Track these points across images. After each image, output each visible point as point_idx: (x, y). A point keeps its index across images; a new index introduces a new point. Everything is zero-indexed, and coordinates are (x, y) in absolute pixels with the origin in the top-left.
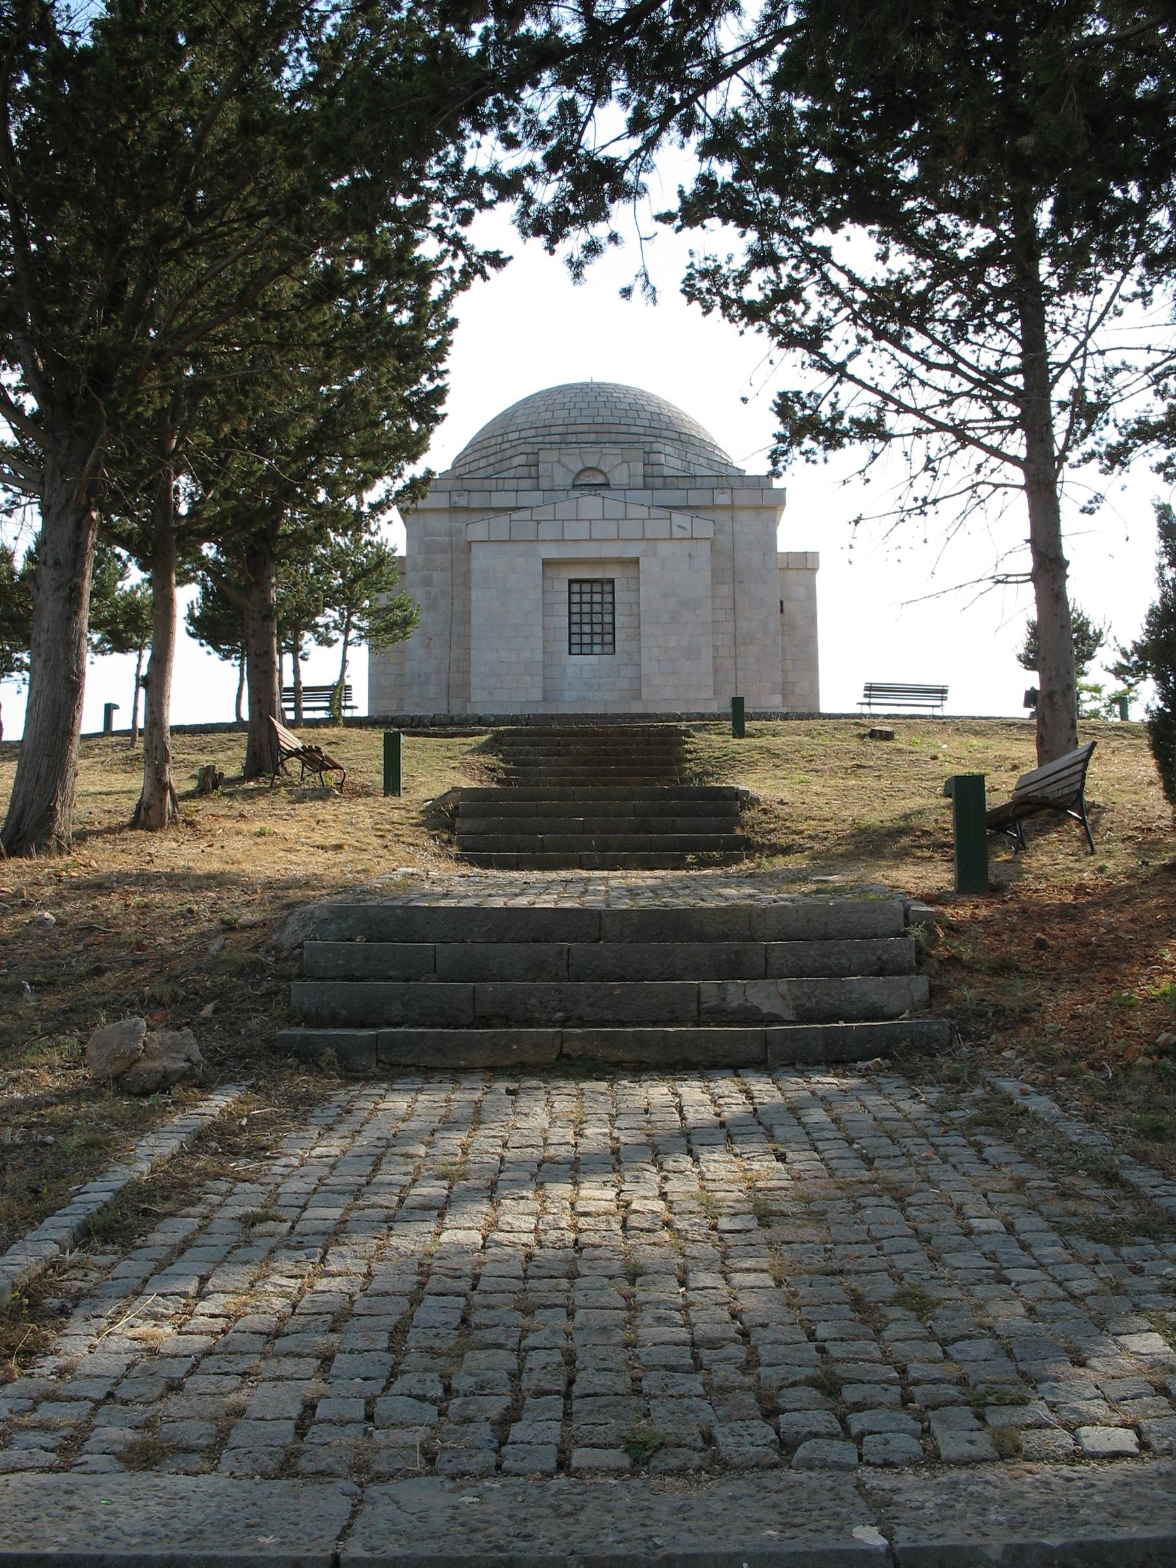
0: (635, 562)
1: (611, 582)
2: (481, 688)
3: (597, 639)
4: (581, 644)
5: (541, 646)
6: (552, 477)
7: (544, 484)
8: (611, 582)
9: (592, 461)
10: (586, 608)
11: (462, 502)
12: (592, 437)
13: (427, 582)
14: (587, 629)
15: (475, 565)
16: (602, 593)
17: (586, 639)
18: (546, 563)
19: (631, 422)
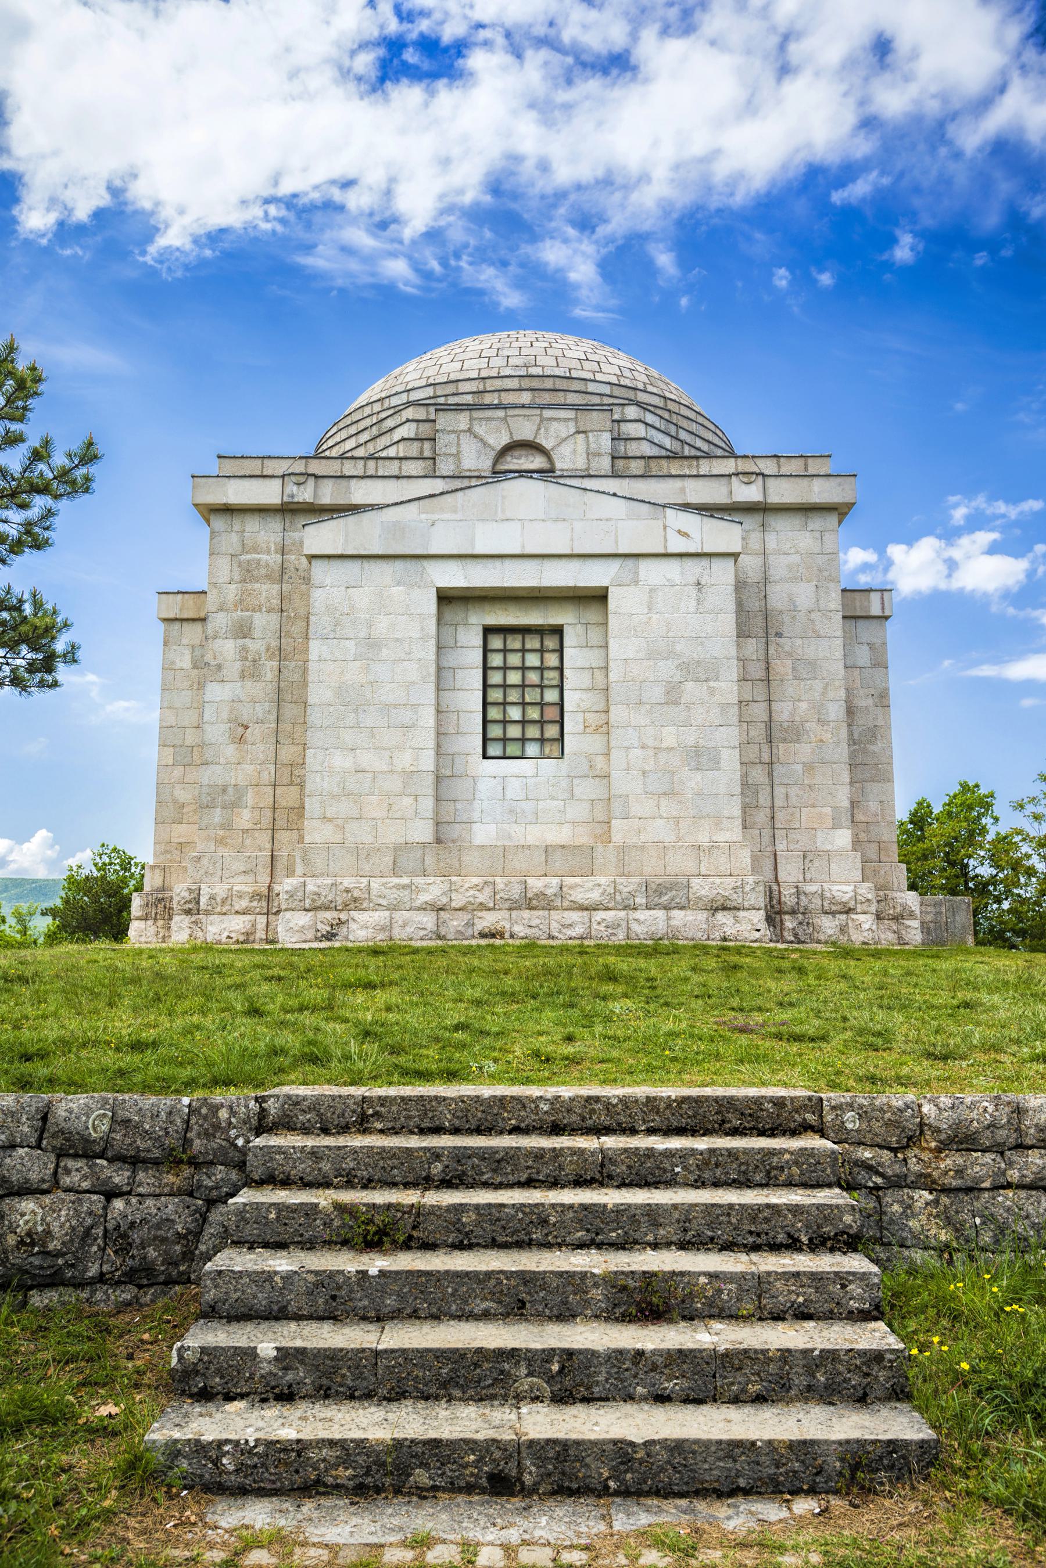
0: (599, 597)
1: (558, 631)
2: (325, 818)
3: (533, 732)
4: (505, 740)
5: (431, 743)
6: (457, 456)
7: (445, 467)
8: (558, 631)
9: (525, 430)
10: (514, 678)
11: (305, 494)
12: (526, 398)
13: (243, 631)
14: (515, 713)
15: (319, 597)
16: (542, 651)
17: (514, 731)
18: (446, 598)
19: (590, 376)
